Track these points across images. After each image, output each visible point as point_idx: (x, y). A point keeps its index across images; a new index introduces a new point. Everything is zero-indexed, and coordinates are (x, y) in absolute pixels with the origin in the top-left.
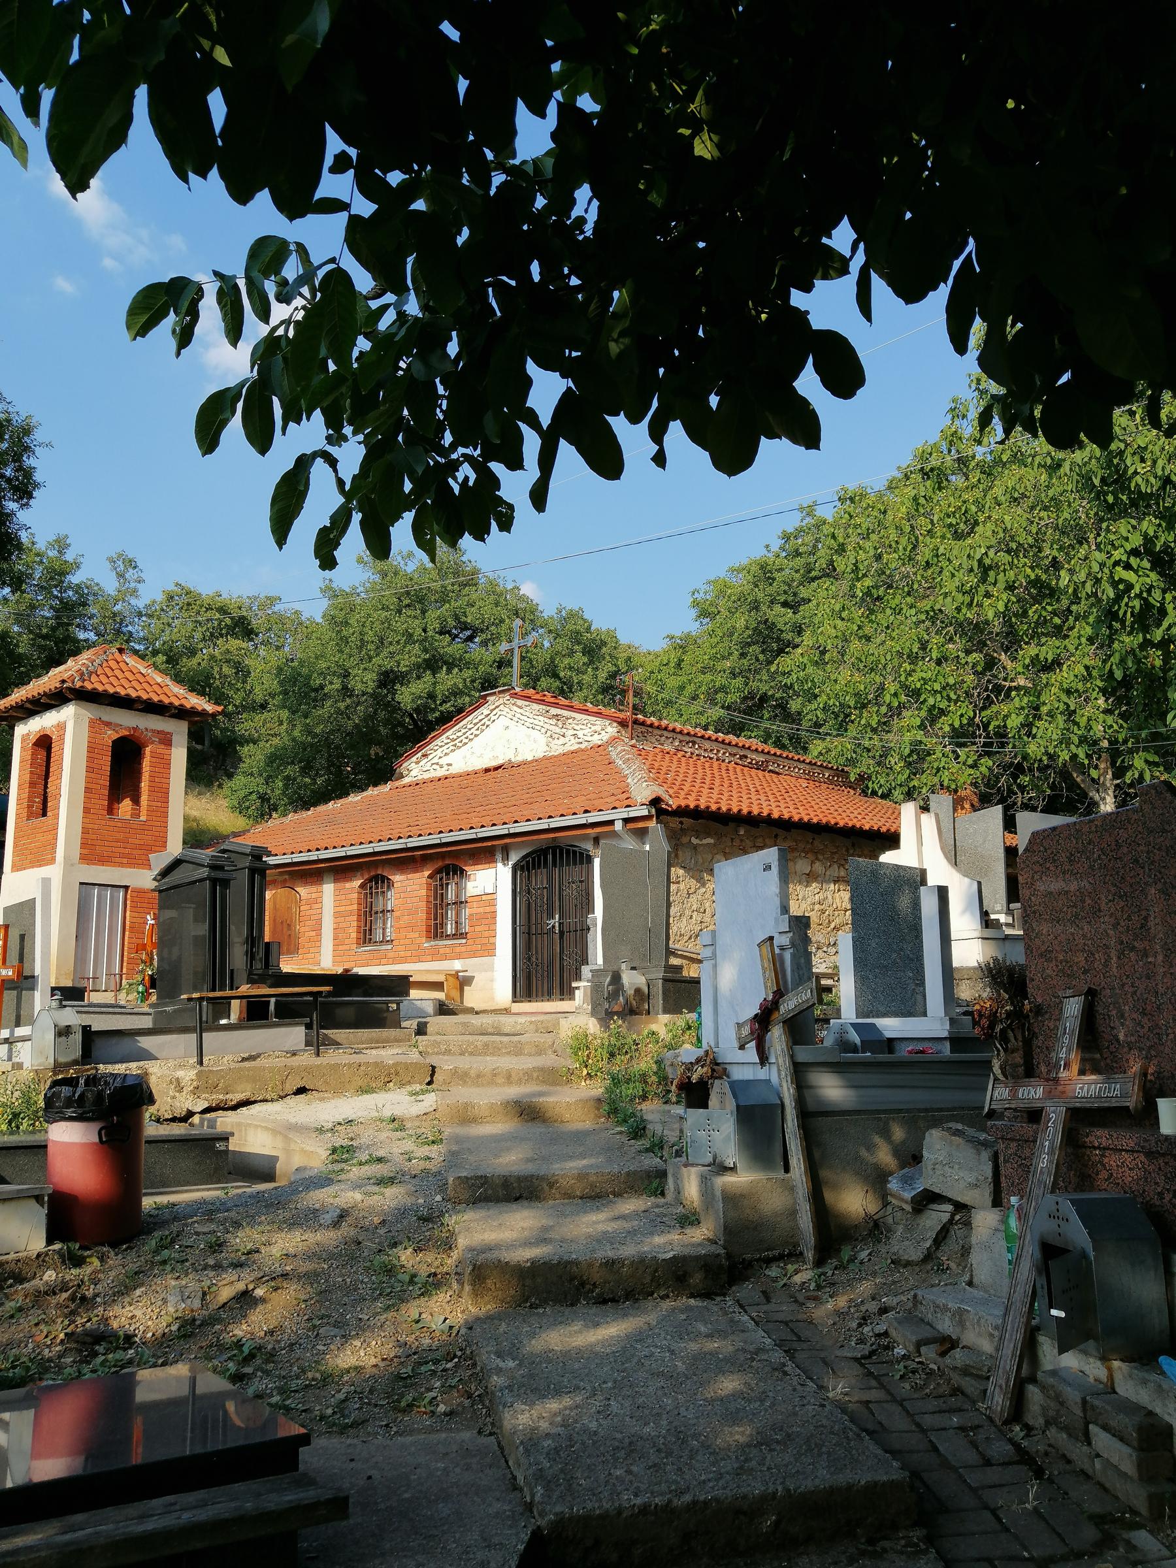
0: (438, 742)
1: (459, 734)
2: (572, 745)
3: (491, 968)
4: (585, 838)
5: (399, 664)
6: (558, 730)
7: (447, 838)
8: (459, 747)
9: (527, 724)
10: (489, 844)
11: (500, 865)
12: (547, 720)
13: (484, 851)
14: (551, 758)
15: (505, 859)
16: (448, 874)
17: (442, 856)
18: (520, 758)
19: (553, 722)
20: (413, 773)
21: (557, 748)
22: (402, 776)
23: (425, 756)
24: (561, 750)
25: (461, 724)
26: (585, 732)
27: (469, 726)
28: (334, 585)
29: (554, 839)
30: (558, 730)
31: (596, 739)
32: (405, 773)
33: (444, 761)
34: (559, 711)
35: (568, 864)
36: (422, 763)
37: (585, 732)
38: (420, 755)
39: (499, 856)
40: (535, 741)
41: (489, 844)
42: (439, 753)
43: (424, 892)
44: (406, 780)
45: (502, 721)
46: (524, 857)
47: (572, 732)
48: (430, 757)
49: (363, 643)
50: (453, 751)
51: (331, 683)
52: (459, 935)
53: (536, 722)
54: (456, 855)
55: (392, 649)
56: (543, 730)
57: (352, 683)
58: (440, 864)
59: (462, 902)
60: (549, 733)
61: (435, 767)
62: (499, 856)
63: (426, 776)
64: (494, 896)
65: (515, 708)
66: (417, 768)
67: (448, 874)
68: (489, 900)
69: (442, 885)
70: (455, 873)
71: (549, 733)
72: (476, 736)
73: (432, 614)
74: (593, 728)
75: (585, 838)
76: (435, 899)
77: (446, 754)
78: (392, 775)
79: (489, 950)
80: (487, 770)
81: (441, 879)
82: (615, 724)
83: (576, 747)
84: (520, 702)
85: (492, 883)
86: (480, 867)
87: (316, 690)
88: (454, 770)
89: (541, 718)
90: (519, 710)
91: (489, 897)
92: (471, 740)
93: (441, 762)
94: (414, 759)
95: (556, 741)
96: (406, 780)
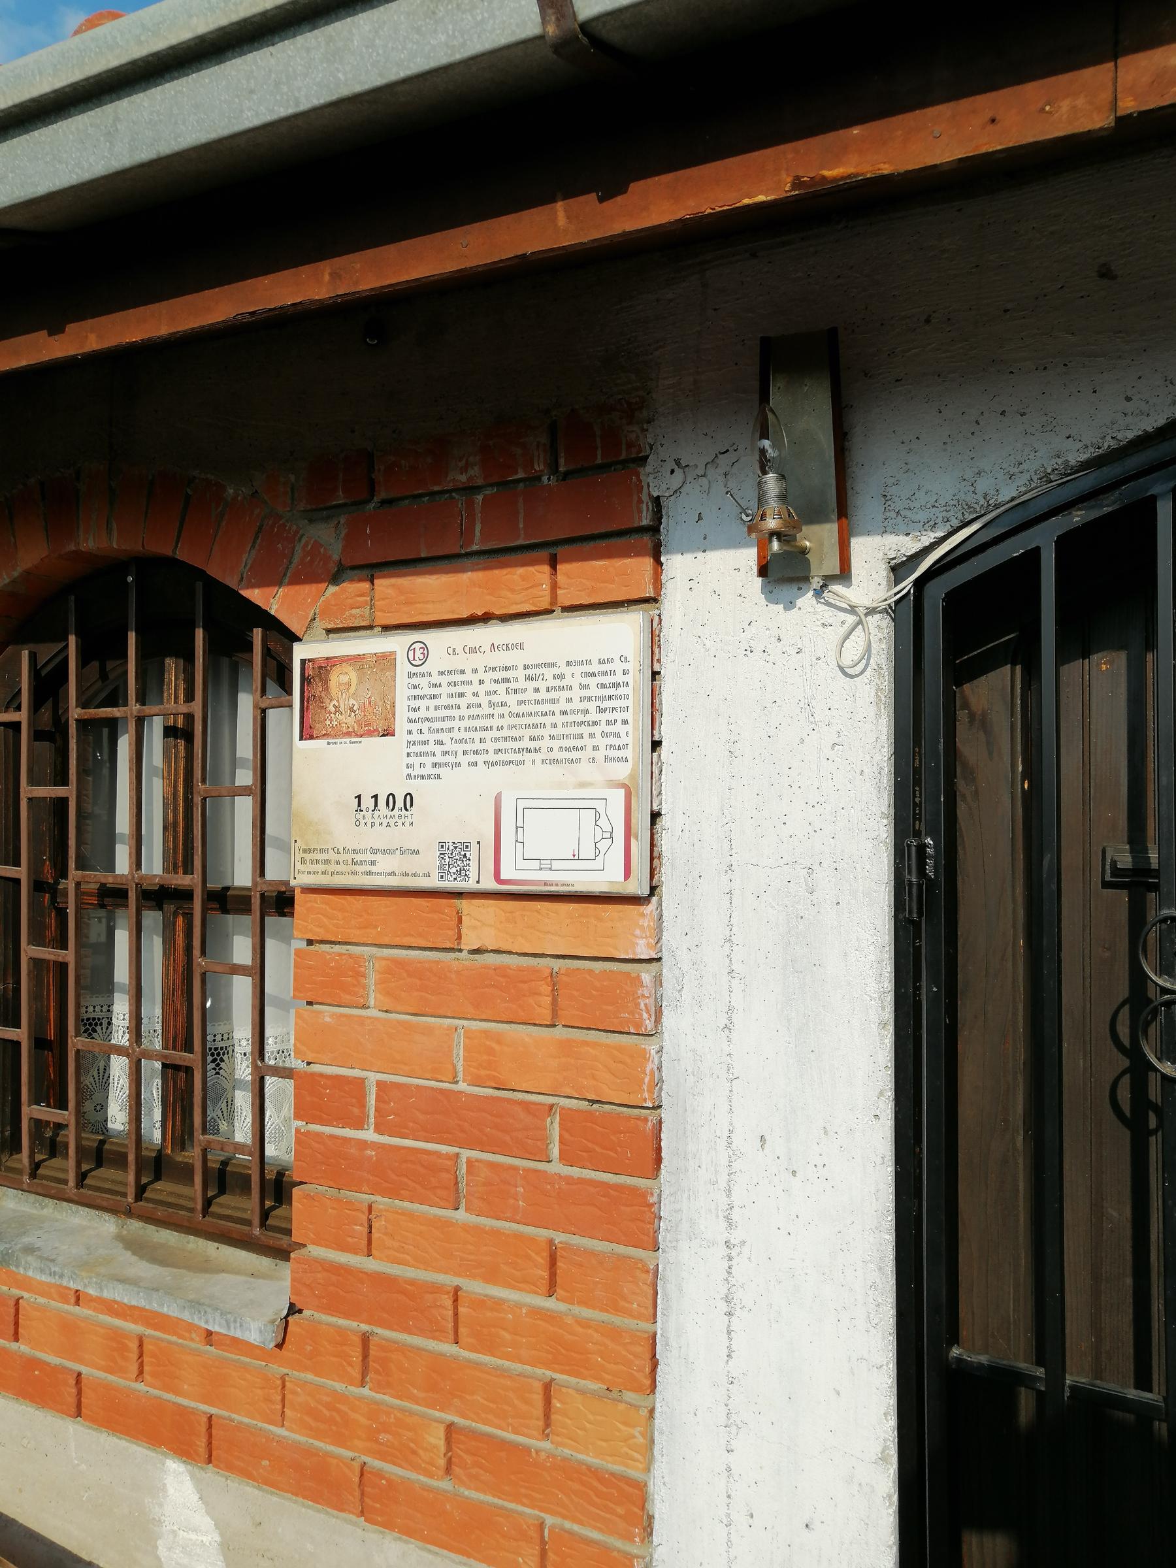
16: (102, 649)
64: (628, 933)
67: (102, 649)
68: (584, 962)
69: (52, 734)
81: (48, 687)
86: (432, 589)
91: (557, 930)
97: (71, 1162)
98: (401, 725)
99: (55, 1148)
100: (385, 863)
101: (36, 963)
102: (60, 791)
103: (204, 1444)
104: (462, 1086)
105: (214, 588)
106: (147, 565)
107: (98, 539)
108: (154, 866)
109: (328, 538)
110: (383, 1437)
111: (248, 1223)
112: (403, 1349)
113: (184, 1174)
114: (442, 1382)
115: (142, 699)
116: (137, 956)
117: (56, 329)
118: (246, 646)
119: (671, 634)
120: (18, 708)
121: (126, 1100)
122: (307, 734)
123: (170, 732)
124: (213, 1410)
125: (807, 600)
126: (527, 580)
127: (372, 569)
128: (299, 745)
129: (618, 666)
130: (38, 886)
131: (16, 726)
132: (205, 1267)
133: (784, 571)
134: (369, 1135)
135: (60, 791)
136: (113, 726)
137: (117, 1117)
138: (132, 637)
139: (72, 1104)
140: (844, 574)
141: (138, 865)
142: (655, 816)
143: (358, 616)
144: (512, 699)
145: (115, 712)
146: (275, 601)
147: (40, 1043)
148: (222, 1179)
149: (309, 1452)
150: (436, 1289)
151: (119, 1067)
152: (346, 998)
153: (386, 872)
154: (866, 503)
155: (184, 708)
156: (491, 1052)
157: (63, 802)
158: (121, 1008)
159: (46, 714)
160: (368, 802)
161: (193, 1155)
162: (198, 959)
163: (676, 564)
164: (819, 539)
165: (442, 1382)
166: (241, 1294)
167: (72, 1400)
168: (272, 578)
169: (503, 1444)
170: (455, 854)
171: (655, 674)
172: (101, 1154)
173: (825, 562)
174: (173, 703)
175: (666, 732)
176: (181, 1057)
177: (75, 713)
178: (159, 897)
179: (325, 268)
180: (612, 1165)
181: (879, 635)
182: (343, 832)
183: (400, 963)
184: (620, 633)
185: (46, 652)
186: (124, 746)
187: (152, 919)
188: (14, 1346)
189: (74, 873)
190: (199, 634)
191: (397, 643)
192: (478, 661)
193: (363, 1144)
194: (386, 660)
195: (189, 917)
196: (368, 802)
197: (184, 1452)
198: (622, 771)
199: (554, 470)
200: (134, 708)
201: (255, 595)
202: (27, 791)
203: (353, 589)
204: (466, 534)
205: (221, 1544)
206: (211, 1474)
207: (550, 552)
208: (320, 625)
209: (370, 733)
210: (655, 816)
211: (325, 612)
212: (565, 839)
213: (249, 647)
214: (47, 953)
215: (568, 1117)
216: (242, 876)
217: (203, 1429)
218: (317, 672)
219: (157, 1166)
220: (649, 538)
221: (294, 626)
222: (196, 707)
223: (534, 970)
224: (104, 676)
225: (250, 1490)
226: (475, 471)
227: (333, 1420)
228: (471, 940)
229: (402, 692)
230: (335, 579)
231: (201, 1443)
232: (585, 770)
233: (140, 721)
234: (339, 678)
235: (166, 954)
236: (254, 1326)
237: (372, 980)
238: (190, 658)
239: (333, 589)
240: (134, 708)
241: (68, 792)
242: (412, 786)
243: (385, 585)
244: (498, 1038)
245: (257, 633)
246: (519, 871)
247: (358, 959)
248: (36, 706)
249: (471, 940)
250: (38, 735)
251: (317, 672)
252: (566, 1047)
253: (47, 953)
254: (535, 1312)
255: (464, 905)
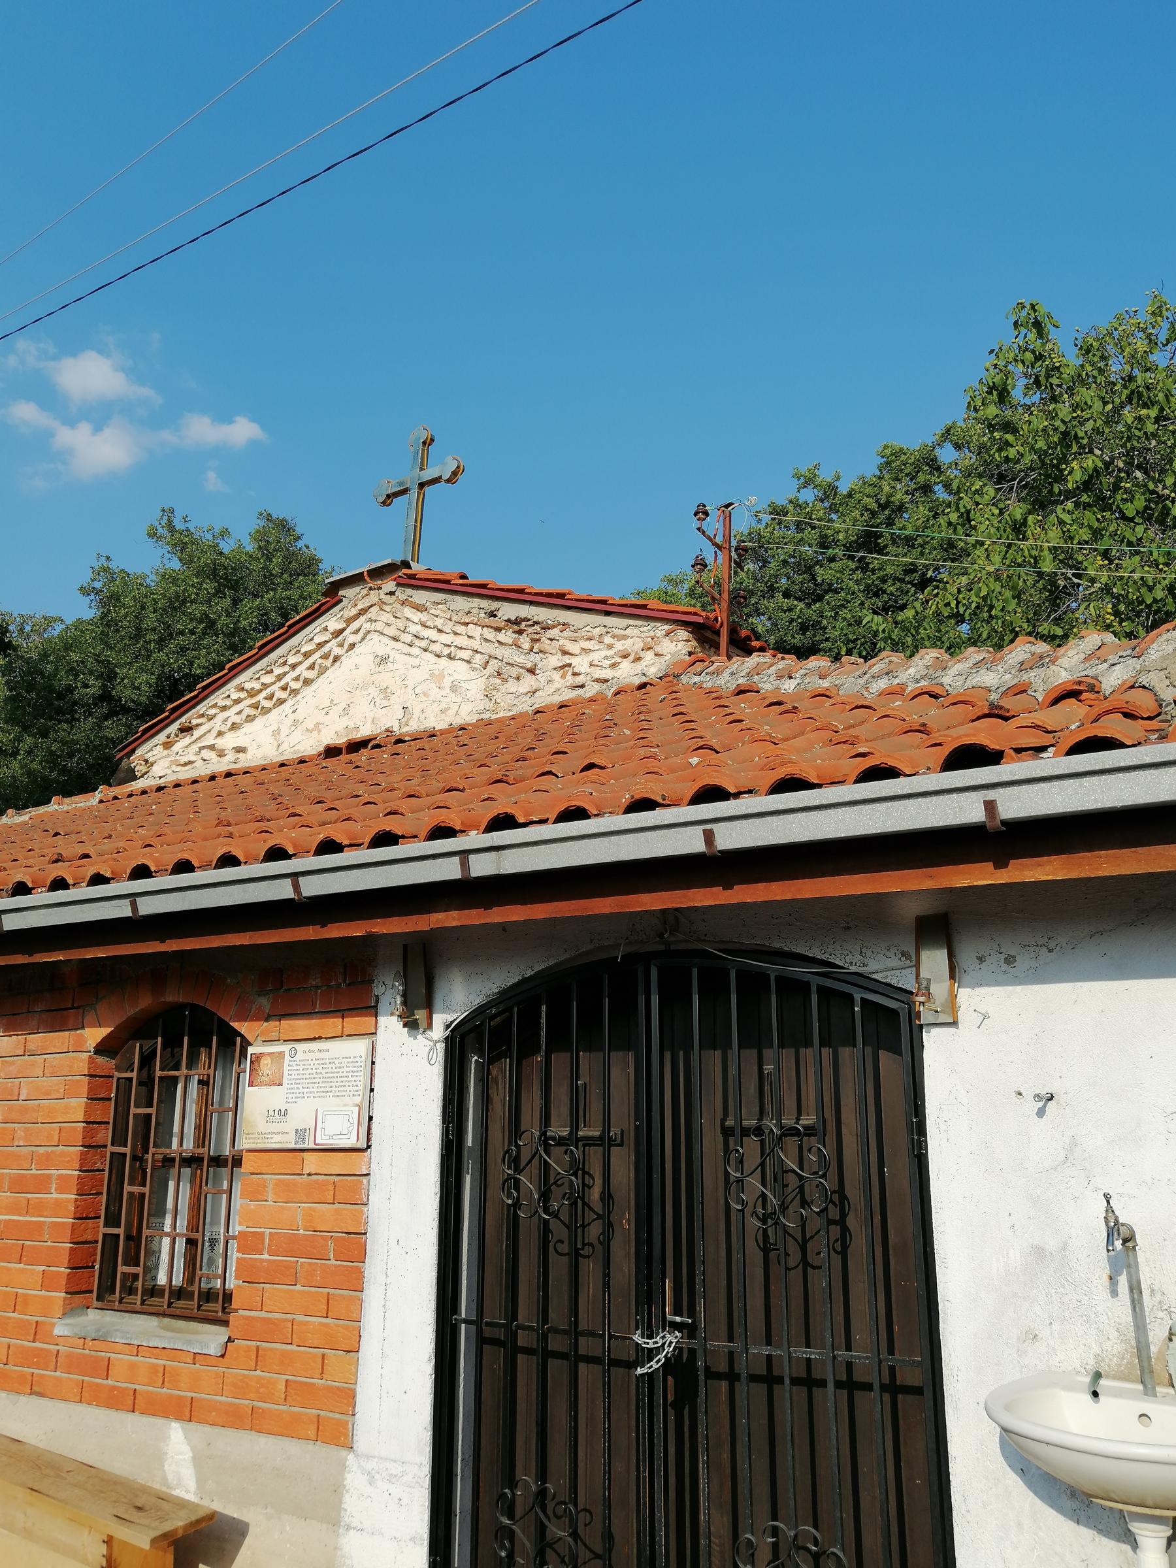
0: (218, 698)
1: (267, 679)
2: (553, 689)
3: (327, 1509)
4: (868, 918)
5: (192, 664)
6: (520, 659)
7: (163, 898)
8: (266, 711)
9: (435, 648)
10: (355, 929)
11: (390, 1026)
12: (489, 634)
13: (327, 959)
14: (489, 723)
15: (417, 1008)
16: (172, 1043)
17: (155, 971)
18: (414, 726)
19: (507, 636)
20: (157, 770)
21: (516, 698)
22: (132, 776)
23: (186, 730)
24: (526, 706)
25: (273, 656)
26: (595, 657)
27: (292, 660)
28: (113, 565)
29: (671, 919)
30: (520, 659)
31: (628, 674)
32: (140, 768)
33: (230, 741)
34: (523, 611)
35: (715, 1039)
36: (178, 747)
37: (595, 657)
38: (175, 726)
39: (390, 994)
40: (454, 688)
41: (355, 929)
42: (217, 724)
43: (76, 1108)
44: (140, 784)
45: (377, 645)
46: (505, 997)
47: (555, 660)
48: (197, 733)
49: (138, 635)
50: (250, 719)
51: (86, 686)
52: (203, 1302)
53: (461, 641)
54: (209, 970)
55: (181, 640)
56: (478, 659)
57: (119, 688)
58: (145, 1002)
59: (218, 1161)
60: (494, 665)
61: (206, 754)
62: (390, 994)
63: (186, 774)
64: (358, 1164)
65: (408, 612)
66: (163, 760)
67: (172, 1043)
68: (341, 1174)
69: (147, 1083)
70: (200, 1041)
71: (494, 665)
72: (307, 682)
73: (248, 604)
74: (619, 646)
75: (868, 918)
76: (119, 1138)
77: (234, 727)
78: (113, 772)
79: (326, 1415)
80: (331, 752)
81: (147, 1060)
82: (683, 634)
83: (568, 695)
84: (420, 597)
85: (357, 1104)
86: (301, 1026)
87: (61, 696)
88: (245, 761)
89: (476, 631)
90: (416, 616)
91: (337, 1164)
92: (295, 692)
93: (221, 743)
94: (162, 737)
95: (512, 686)
96: (140, 784)
97: (139, 1297)
98: (285, 1081)
99: (131, 1291)
100: (277, 1138)
101: (131, 1194)
102: (148, 1111)
103: (187, 1411)
104: (302, 1231)
105: (221, 1020)
106: (193, 1007)
107: (173, 996)
108: (189, 1144)
109: (265, 1003)
110: (262, 1390)
111: (217, 1312)
112: (271, 1349)
113: (190, 1295)
114: (286, 1361)
115: (189, 1067)
116: (179, 1193)
117: (163, 941)
118: (231, 1045)
119: (379, 1048)
120: (132, 1071)
121: (168, 1268)
122: (251, 1085)
123: (200, 1082)
124: (193, 1395)
125: (420, 1037)
126: (333, 1024)
127: (281, 1016)
128: (248, 1089)
129: (359, 1059)
130: (134, 1158)
131: (131, 1079)
132: (197, 1333)
133: (411, 1025)
134: (266, 1257)
135: (148, 1111)
136: (175, 1080)
137: (162, 1279)
138: (186, 1038)
139: (142, 1264)
140: (430, 1026)
141: (181, 1145)
142: (370, 1118)
143: (274, 1035)
144: (324, 1071)
145: (176, 1073)
146: (242, 1027)
147: (129, 1237)
148: (208, 1296)
149: (232, 1404)
150: (285, 1320)
151: (166, 1241)
152: (260, 1197)
153: (275, 1142)
154: (438, 1002)
155: (206, 1072)
156: (311, 1215)
157: (150, 1115)
158: (168, 1221)
159: (145, 1072)
160: (271, 1113)
161: (195, 1288)
162: (204, 1188)
163: (382, 1020)
164: (420, 1015)
165: (286, 1361)
166: (210, 1339)
167: (130, 1402)
168: (243, 1018)
169: (306, 1383)
170: (300, 1133)
171: (373, 1063)
172: (154, 1291)
173: (423, 1024)
174: (201, 1070)
175: (376, 1086)
176: (194, 1235)
177: (158, 1073)
178: (192, 1161)
179: (248, 934)
180: (346, 1255)
181: (441, 1047)
182: (262, 1126)
183: (280, 1180)
184: (360, 1047)
185: (148, 1044)
186: (180, 1087)
187: (186, 1172)
188: (105, 1382)
189: (152, 1150)
190: (215, 1038)
191: (285, 1048)
192: (313, 1056)
193: (263, 1260)
194: (282, 1054)
195: (202, 1170)
196: (271, 1113)
197: (179, 1418)
198: (358, 1100)
199: (344, 981)
200: (184, 1071)
201: (235, 1025)
202: (134, 1110)
203: (273, 1024)
204: (314, 1005)
205: (194, 1458)
206: (192, 1426)
207: (343, 1013)
208: (260, 1039)
209: (274, 1085)
210: (370, 1118)
211: (262, 1033)
212: (340, 1129)
213: (235, 1045)
214: (136, 1189)
215: (337, 1241)
216: (227, 1152)
217: (188, 1404)
218: (256, 1059)
219: (179, 1294)
220: (372, 1009)
221: (250, 1038)
222: (211, 1071)
223: (328, 1181)
224: (173, 1055)
225: (207, 1429)
226: (318, 980)
227: (241, 1389)
228: (306, 1171)
229: (286, 1068)
230: (267, 1020)
231: (187, 1410)
232: (347, 1100)
233: (187, 1078)
234: (265, 1062)
235: (191, 1189)
236: (212, 1346)
237: (270, 1189)
238: (211, 1048)
239: (266, 1024)
240: (184, 1071)
241: (152, 1111)
242: (287, 1106)
243: (285, 1023)
244: (314, 1210)
245: (239, 1039)
246: (323, 1141)
247: (265, 1180)
248: (141, 1069)
249: (306, 1171)
250: (140, 1083)
251: (256, 1059)
252: (337, 1210)
253: (136, 1189)
254: (321, 1324)
255: (305, 1155)
